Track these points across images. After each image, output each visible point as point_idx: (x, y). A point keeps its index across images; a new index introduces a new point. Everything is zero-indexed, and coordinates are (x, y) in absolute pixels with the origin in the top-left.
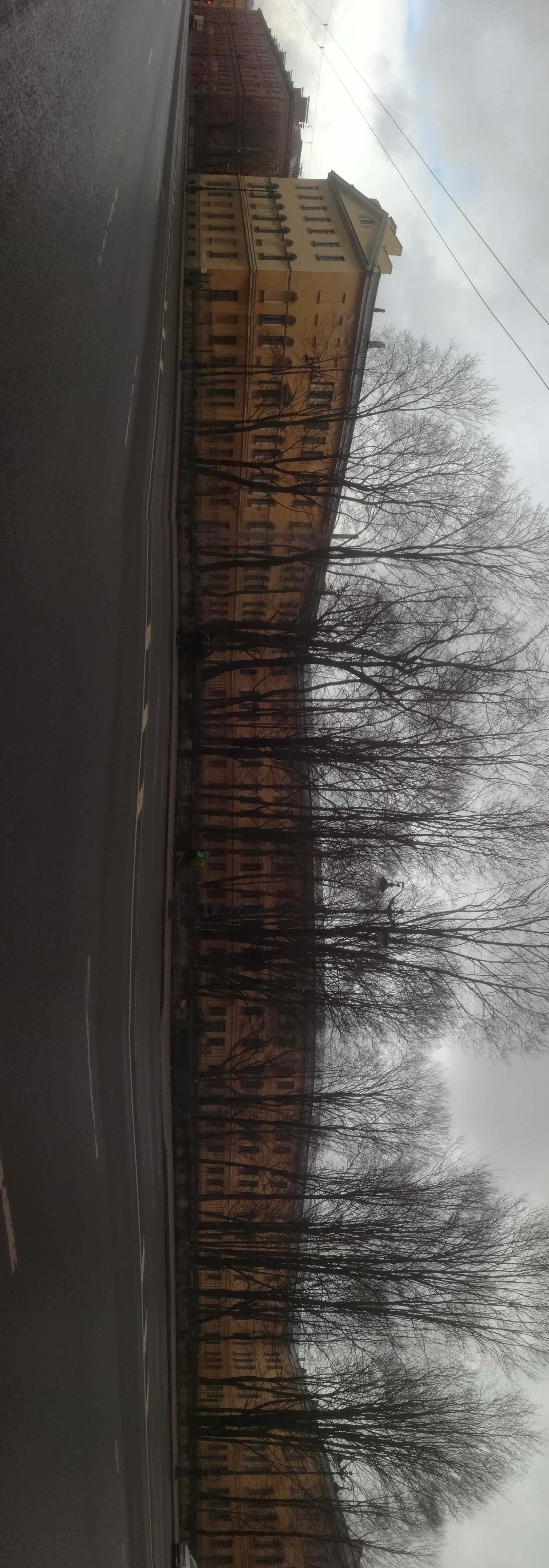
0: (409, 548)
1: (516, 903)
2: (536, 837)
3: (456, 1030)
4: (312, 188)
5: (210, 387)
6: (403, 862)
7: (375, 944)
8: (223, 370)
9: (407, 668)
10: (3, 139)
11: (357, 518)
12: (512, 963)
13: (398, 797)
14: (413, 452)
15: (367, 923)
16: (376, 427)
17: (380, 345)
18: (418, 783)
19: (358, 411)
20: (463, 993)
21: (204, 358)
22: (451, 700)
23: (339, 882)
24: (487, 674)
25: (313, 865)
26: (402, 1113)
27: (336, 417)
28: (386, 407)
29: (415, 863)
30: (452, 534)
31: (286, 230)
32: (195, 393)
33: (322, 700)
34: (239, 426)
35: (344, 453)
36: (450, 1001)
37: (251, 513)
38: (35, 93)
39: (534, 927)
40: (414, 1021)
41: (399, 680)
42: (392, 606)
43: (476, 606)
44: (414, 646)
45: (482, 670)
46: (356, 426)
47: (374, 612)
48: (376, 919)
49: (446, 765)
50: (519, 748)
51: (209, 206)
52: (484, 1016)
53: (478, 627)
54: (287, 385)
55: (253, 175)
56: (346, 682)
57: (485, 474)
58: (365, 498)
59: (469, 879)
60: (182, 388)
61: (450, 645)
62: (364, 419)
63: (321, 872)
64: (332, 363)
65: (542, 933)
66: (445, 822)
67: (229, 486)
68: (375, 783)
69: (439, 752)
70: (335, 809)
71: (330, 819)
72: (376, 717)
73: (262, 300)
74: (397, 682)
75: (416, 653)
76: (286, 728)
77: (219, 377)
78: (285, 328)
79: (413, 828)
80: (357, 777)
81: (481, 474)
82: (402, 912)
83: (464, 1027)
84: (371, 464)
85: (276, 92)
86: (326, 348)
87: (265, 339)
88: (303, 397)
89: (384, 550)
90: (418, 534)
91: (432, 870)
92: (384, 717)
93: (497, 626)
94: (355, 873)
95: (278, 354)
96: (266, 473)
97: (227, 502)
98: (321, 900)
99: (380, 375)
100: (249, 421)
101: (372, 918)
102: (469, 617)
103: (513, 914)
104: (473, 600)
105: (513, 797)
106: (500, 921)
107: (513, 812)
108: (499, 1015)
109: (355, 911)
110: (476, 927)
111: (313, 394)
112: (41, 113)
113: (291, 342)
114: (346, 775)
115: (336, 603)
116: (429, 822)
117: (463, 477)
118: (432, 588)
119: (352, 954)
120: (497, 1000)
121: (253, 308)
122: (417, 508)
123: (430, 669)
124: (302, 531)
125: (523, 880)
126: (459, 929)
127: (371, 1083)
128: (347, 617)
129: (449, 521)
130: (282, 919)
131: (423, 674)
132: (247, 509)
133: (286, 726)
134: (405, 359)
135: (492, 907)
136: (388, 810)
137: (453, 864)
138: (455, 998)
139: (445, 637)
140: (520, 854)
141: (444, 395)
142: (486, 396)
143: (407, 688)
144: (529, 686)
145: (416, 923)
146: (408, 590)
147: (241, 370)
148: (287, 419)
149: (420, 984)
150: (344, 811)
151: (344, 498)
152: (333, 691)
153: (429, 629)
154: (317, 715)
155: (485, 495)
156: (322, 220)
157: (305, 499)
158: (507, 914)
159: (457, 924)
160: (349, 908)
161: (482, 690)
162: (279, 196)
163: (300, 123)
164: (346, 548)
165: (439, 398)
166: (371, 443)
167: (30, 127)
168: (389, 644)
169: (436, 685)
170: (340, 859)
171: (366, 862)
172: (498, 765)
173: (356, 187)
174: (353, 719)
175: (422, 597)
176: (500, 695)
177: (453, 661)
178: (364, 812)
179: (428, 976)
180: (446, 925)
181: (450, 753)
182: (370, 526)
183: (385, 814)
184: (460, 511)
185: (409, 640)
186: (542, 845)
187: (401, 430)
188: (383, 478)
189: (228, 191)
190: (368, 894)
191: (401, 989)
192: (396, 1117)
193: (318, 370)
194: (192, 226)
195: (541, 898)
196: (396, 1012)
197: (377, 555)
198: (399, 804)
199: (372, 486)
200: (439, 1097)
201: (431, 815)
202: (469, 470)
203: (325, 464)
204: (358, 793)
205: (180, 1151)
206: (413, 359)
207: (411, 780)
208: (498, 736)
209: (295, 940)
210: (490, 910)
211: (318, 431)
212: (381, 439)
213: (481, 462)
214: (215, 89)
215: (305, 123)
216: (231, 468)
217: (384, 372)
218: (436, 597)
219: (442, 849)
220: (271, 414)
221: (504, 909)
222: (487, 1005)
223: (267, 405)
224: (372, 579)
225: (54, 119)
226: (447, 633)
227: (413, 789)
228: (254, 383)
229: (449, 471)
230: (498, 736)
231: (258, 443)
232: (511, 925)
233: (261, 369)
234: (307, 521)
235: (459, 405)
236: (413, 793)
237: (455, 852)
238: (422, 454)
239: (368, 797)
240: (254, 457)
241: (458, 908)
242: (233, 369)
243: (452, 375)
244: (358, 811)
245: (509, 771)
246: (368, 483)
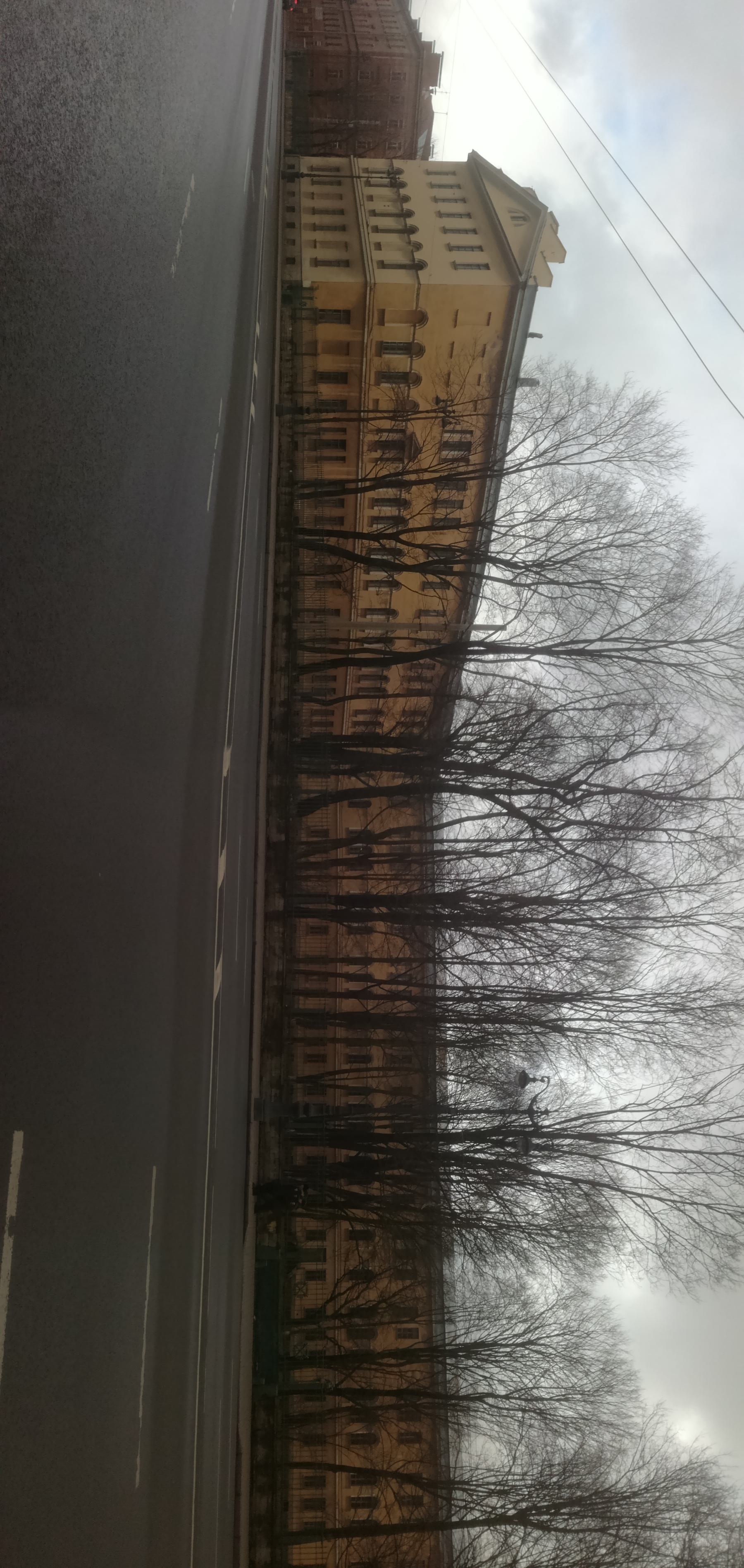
0: (573, 642)
1: (691, 1101)
2: (721, 1020)
3: (622, 1257)
4: (446, 174)
5: (314, 437)
6: (549, 1053)
7: (513, 1151)
8: (331, 416)
9: (570, 796)
10: (47, 111)
11: (504, 605)
12: (689, 1173)
13: (547, 972)
14: (577, 518)
15: (504, 1126)
16: (529, 487)
17: (532, 383)
18: (575, 954)
19: (506, 466)
20: (627, 1211)
21: (306, 400)
22: (626, 839)
23: (468, 1076)
24: (674, 803)
25: (436, 1056)
26: (571, 1371)
27: (477, 475)
28: (542, 460)
29: (564, 1052)
30: (629, 623)
31: (413, 230)
32: (295, 445)
33: (456, 841)
34: (352, 486)
35: (488, 520)
36: (613, 1221)
37: (368, 598)
38: (87, 50)
39: (714, 1129)
40: (568, 1246)
41: (558, 813)
42: (550, 716)
43: (657, 715)
44: (578, 766)
45: (667, 799)
46: (502, 485)
47: (526, 723)
48: (513, 1122)
49: (613, 929)
50: (711, 904)
51: (313, 198)
52: (657, 1239)
53: (660, 742)
54: (413, 434)
55: (371, 158)
56: (488, 816)
57: (672, 546)
58: (515, 578)
59: (632, 1073)
60: (279, 439)
61: (625, 765)
62: (513, 476)
63: (445, 1065)
64: (471, 406)
65: (724, 1137)
66: (606, 1002)
67: (339, 563)
68: (520, 954)
69: (605, 910)
70: (466, 988)
71: (460, 1000)
72: (527, 863)
73: (382, 322)
74: (556, 815)
75: (581, 776)
76: (408, 880)
77: (325, 425)
78: (412, 360)
79: (564, 1011)
80: (497, 947)
81: (666, 545)
82: (547, 1112)
83: (633, 1253)
84: (523, 534)
85: (399, 47)
86: (462, 387)
87: (385, 376)
88: (434, 449)
89: (539, 645)
90: (584, 625)
91: (586, 1061)
92: (538, 863)
93: (686, 742)
94: (488, 1066)
95: (401, 395)
96: (387, 546)
97: (338, 585)
98: (445, 1098)
99: (533, 420)
100: (364, 480)
101: (509, 1120)
102: (649, 730)
103: (687, 1114)
104: (653, 708)
105: (695, 970)
106: (671, 1122)
107: (694, 989)
108: (677, 1237)
109: (487, 1111)
110: (640, 1130)
111: (445, 445)
112: (95, 75)
113: (418, 380)
114: (482, 944)
115: (476, 712)
116: (585, 1003)
117: (643, 550)
118: (601, 693)
119: (486, 1164)
120: (673, 1219)
121: (370, 332)
122: (583, 590)
123: (600, 797)
124: (432, 620)
125: (701, 1074)
126: (619, 1133)
127: (520, 1328)
128: (490, 731)
129: (626, 606)
130: (397, 1121)
131: (590, 804)
132: (363, 593)
133: (408, 877)
134: (565, 400)
135: (661, 1106)
136: (533, 989)
137: (613, 1055)
138: (619, 1218)
139: (619, 755)
140: (699, 1042)
141: (617, 444)
142: (672, 444)
143: (569, 823)
144: (728, 820)
145: (564, 1125)
146: (570, 695)
147: (354, 415)
148: (413, 477)
149: (572, 1199)
150: (477, 991)
151: (489, 578)
152: (471, 827)
153: (598, 745)
154: (449, 861)
155: (672, 573)
156: (461, 216)
157: (438, 580)
158: (680, 1115)
159: (617, 1127)
160: (480, 1107)
161: (667, 826)
162: (403, 185)
163: (431, 88)
164: (490, 643)
165: (610, 448)
166: (522, 507)
167: (81, 95)
168: (545, 764)
169: (607, 819)
170: (470, 1049)
171: (503, 1053)
172: (681, 928)
173: (505, 171)
174: (496, 866)
175: (587, 704)
176: (691, 832)
177: (629, 787)
178: (502, 992)
179: (582, 1190)
180: (603, 1128)
181: (621, 913)
182: (522, 615)
183: (529, 993)
184: (640, 593)
185: (572, 759)
186: (727, 1030)
187: (561, 490)
188: (538, 552)
189: (336, 178)
190: (505, 1091)
191: (549, 1206)
192: (563, 1377)
193: (452, 414)
194: (291, 225)
195: (722, 1095)
196: (543, 1235)
197: (530, 651)
198: (548, 981)
199: (524, 562)
200: (614, 1345)
201: (588, 994)
202: (651, 540)
203: (463, 534)
204: (496, 967)
205: (261, 1452)
206: (575, 399)
207: (566, 950)
208: (685, 888)
209: (412, 1146)
210: (658, 1110)
211: (454, 491)
212: (536, 502)
213: (667, 530)
214: (319, 43)
215: (437, 88)
216: (341, 540)
217: (538, 416)
218: (606, 704)
219: (600, 1036)
220: (392, 471)
221: (675, 1108)
222: (659, 1225)
223: (388, 460)
224: (524, 681)
225: (111, 84)
226: (620, 750)
227: (567, 961)
228: (371, 431)
229: (625, 542)
230: (685, 888)
231: (376, 508)
232: (686, 1127)
233: (379, 415)
234: (440, 608)
235: (637, 457)
236: (568, 966)
237: (617, 1039)
238: (589, 521)
239: (509, 973)
240: (371, 526)
241: (618, 1107)
242: (344, 415)
243: (627, 419)
244: (495, 990)
245: (695, 936)
246: (517, 559)
